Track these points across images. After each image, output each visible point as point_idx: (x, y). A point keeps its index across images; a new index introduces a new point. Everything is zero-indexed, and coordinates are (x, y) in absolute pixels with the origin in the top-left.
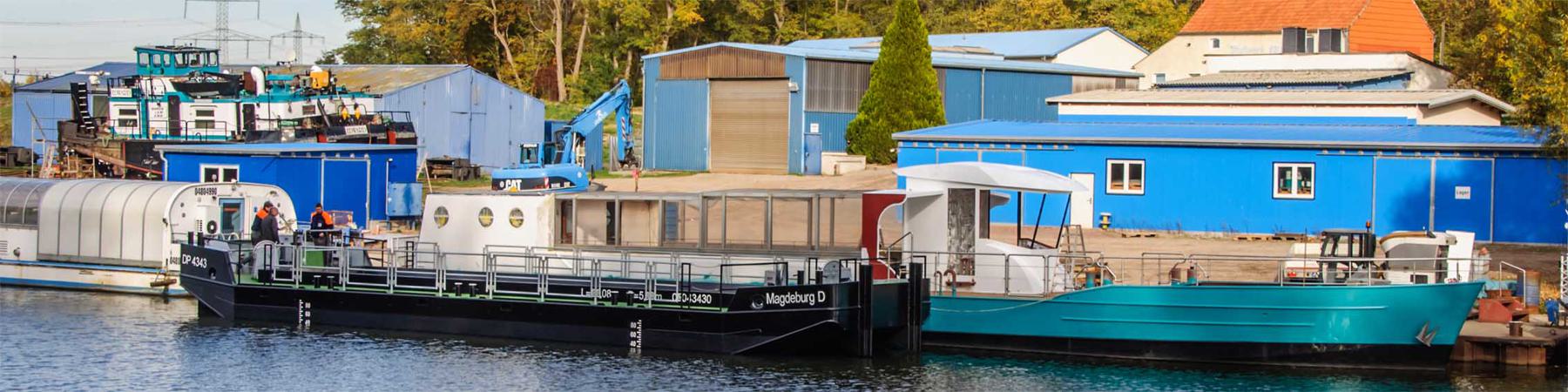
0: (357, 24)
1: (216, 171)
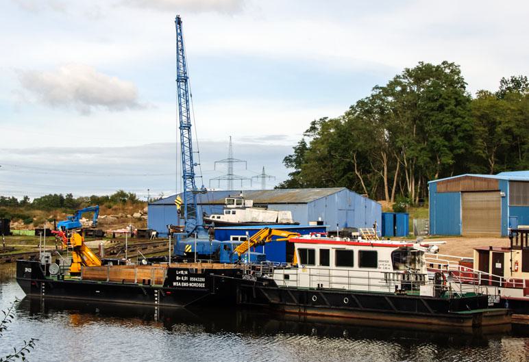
0: (293, 170)
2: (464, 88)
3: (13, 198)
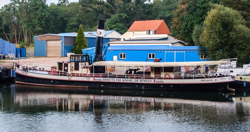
2: (46, 2)
3: (242, 67)
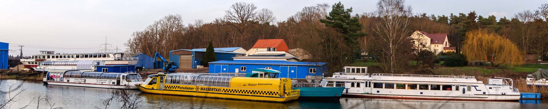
1: (349, 69)
